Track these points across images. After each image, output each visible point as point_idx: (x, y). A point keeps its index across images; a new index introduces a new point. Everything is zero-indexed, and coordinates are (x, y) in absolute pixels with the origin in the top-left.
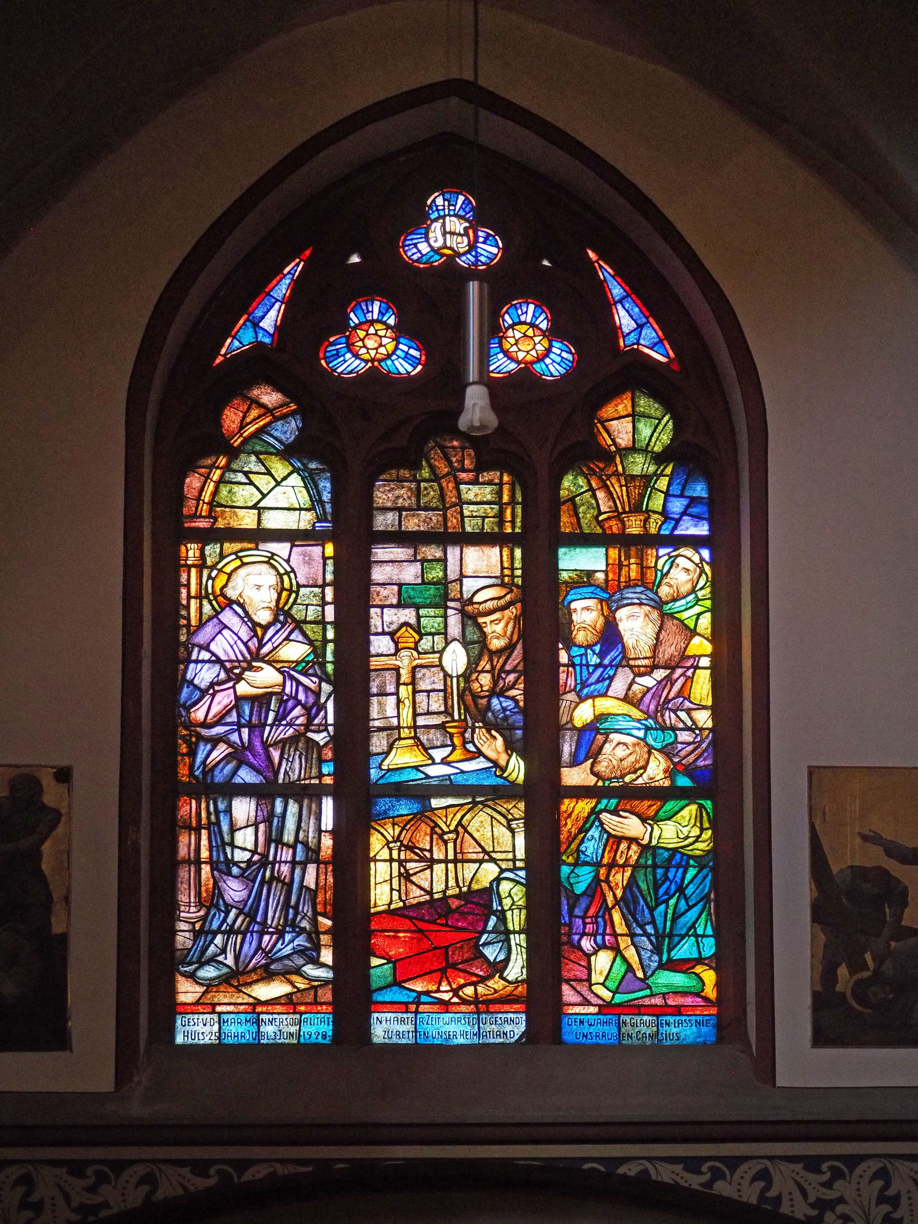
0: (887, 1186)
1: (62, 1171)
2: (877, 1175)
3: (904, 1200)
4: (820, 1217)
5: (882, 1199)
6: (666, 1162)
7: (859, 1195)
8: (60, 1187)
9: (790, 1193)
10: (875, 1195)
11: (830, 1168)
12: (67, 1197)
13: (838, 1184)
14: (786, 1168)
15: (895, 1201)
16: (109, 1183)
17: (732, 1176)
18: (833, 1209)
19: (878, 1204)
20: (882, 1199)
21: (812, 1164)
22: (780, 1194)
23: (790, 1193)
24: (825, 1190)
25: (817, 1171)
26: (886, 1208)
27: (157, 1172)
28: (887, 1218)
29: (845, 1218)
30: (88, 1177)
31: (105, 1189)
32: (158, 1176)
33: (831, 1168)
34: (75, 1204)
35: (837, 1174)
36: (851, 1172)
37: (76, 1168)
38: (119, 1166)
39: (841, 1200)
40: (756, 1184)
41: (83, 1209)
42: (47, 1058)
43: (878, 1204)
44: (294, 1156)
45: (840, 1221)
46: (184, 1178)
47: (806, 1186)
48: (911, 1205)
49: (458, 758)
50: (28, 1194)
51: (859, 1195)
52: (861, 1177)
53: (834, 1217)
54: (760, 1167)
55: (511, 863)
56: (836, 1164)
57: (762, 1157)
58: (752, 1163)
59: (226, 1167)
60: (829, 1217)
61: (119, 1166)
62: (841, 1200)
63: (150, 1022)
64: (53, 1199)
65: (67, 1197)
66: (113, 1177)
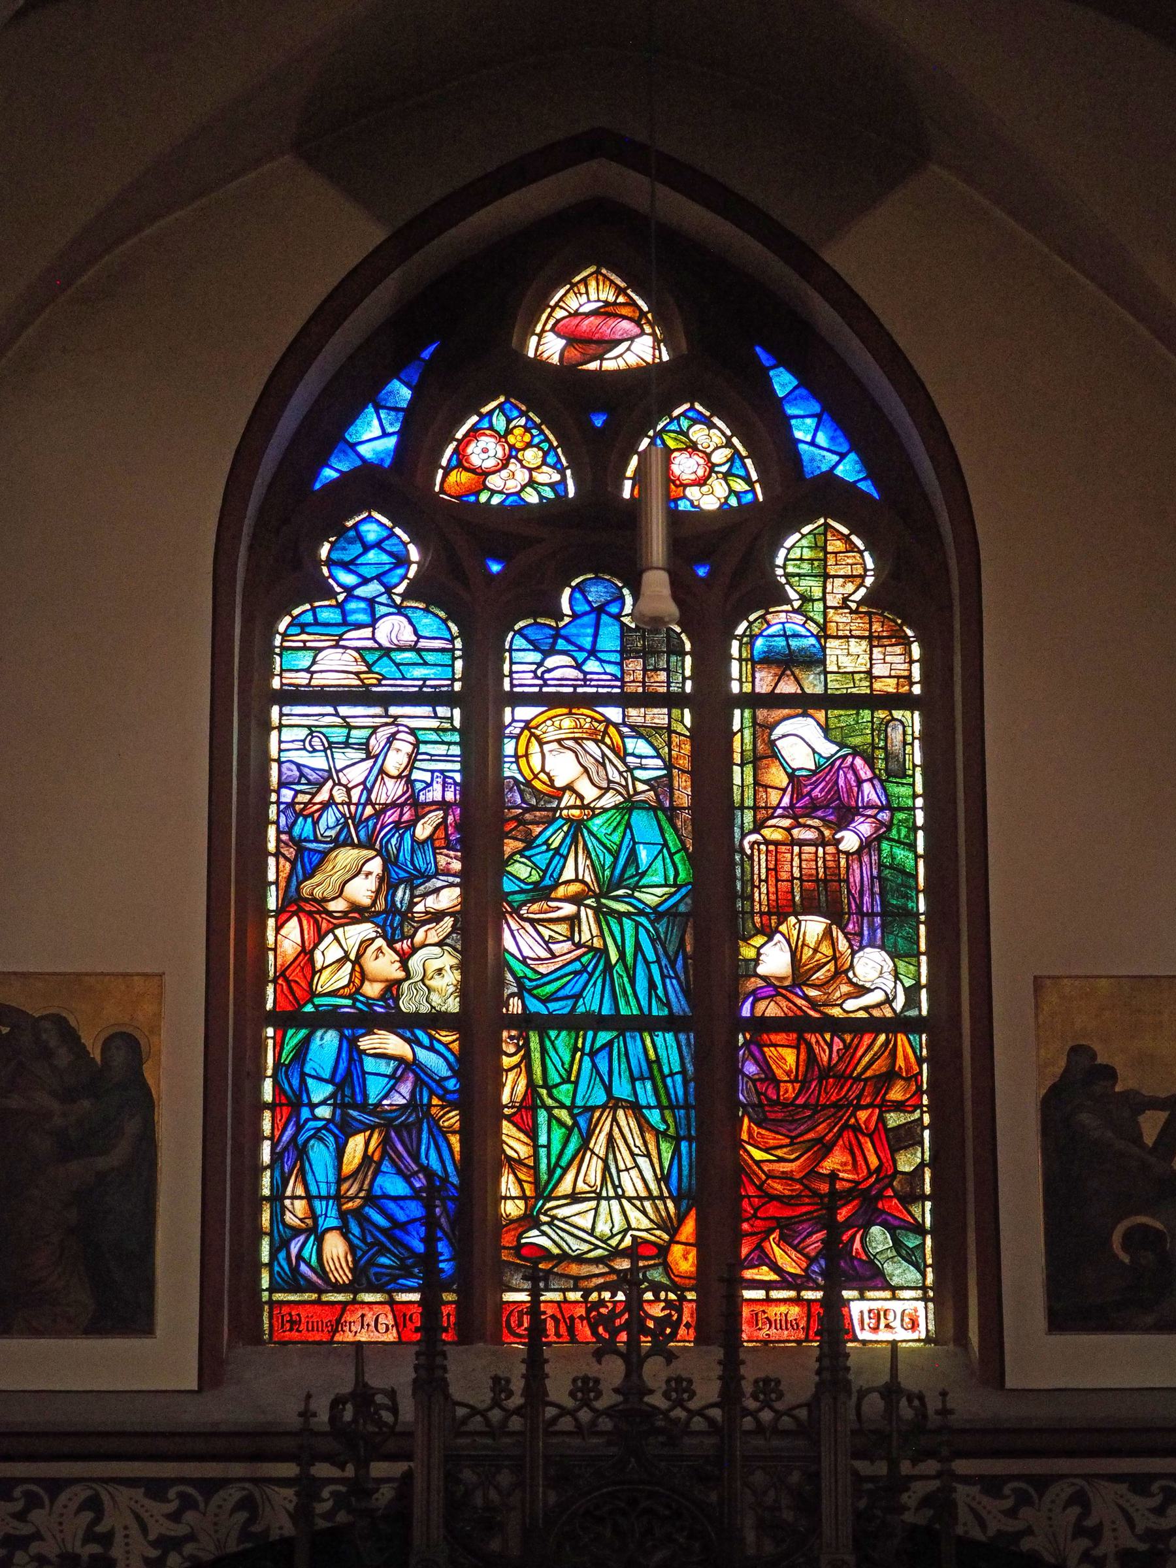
0: (98, 1520)
1: (1123, 1488)
2: (241, 1505)
3: (118, 1539)
4: (162, 1560)
5: (1080, 1531)
6: (278, 1485)
7: (61, 1531)
8: (1120, 1507)
9: (126, 1528)
10: (80, 1534)
11: (332, 1493)
12: (144, 1529)
13: (190, 1516)
14: (124, 1495)
15: (1095, 1534)
16: (42, 1506)
17: (52, 1502)
18: (25, 1548)
19: (1074, 1537)
20: (1080, 1531)
21: (156, 1488)
22: (1101, 1523)
23: (126, 1528)
24: (16, 1523)
25: (1144, 1492)
26: (1084, 1543)
27: (257, 1495)
28: (1086, 1556)
29: (41, 1559)
30: (169, 1501)
31: (37, 1515)
32: (259, 1500)
33: (1163, 1489)
34: (1140, 1528)
35: (1023, 1499)
36: (1041, 1496)
37: (156, 1488)
38: (55, 1486)
39: (37, 1536)
40: (1068, 1511)
41: (166, 1544)
42: (1040, 1319)
43: (1074, 1537)
44: (1111, 1470)
45: (35, 1564)
46: (137, 1502)
47: (984, 1514)
48: (127, 1544)
49: (382, 607)
50: (1081, 1517)
51: (61, 1531)
52: (65, 1507)
53: (27, 1559)
54: (89, 1493)
55: (746, 916)
56: (190, 1490)
57: (1076, 1476)
58: (77, 1488)
59: (34, 1488)
60: (20, 1557)
61: (1042, 1483)
62: (37, 1536)
63: (965, 1255)
64: (1113, 1522)
65: (144, 1529)
66: (200, 1498)
